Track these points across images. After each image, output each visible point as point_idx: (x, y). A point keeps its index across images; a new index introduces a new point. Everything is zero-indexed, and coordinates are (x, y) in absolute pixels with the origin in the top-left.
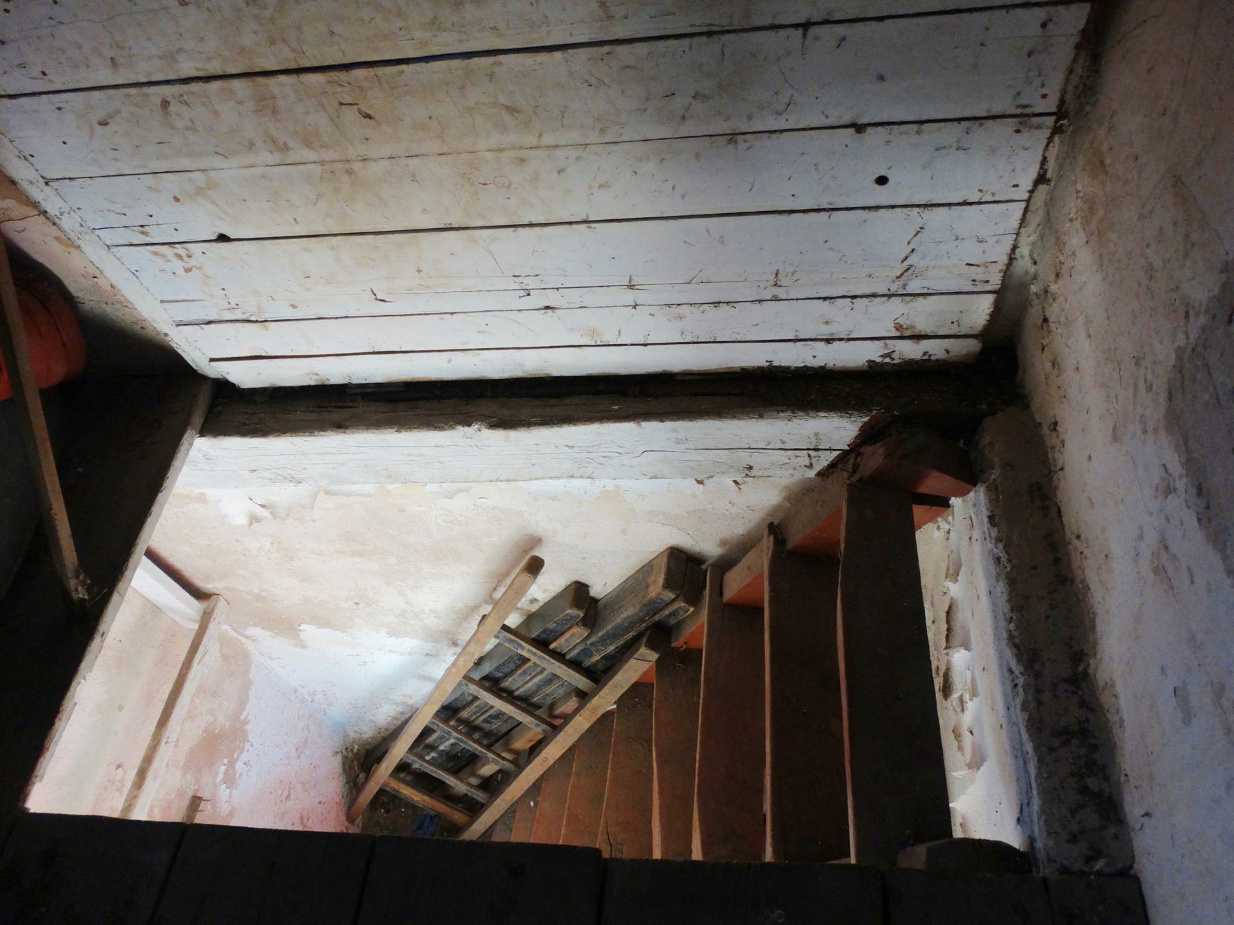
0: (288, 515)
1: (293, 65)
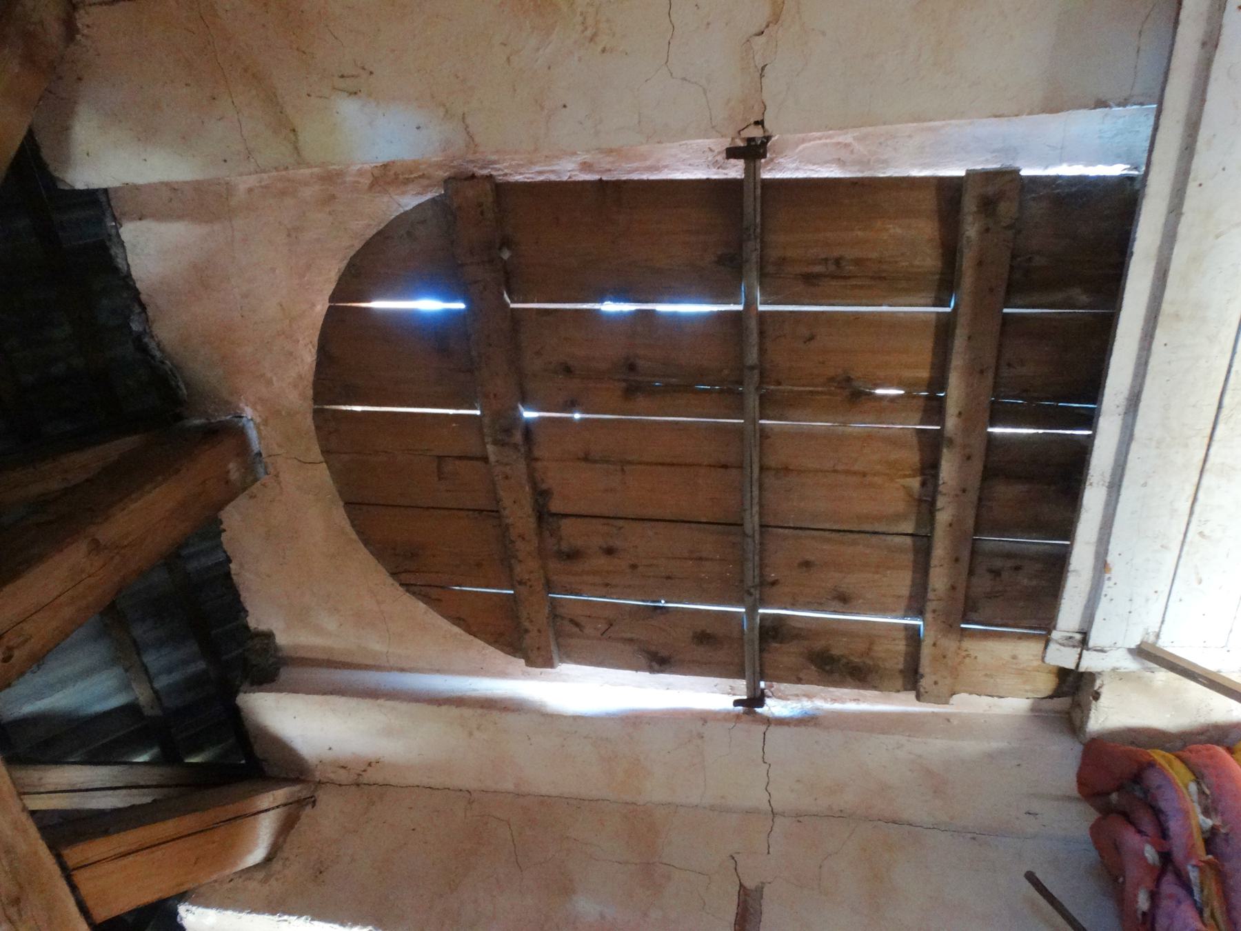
0: (21, 887)
1: (1206, 441)
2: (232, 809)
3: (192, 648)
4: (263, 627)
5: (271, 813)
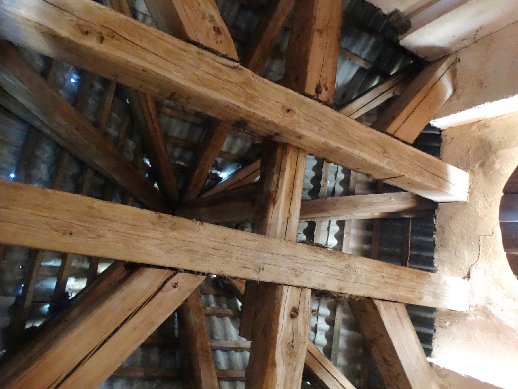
2: (429, 84)
3: (366, 36)
4: (391, 10)
5: (445, 75)
